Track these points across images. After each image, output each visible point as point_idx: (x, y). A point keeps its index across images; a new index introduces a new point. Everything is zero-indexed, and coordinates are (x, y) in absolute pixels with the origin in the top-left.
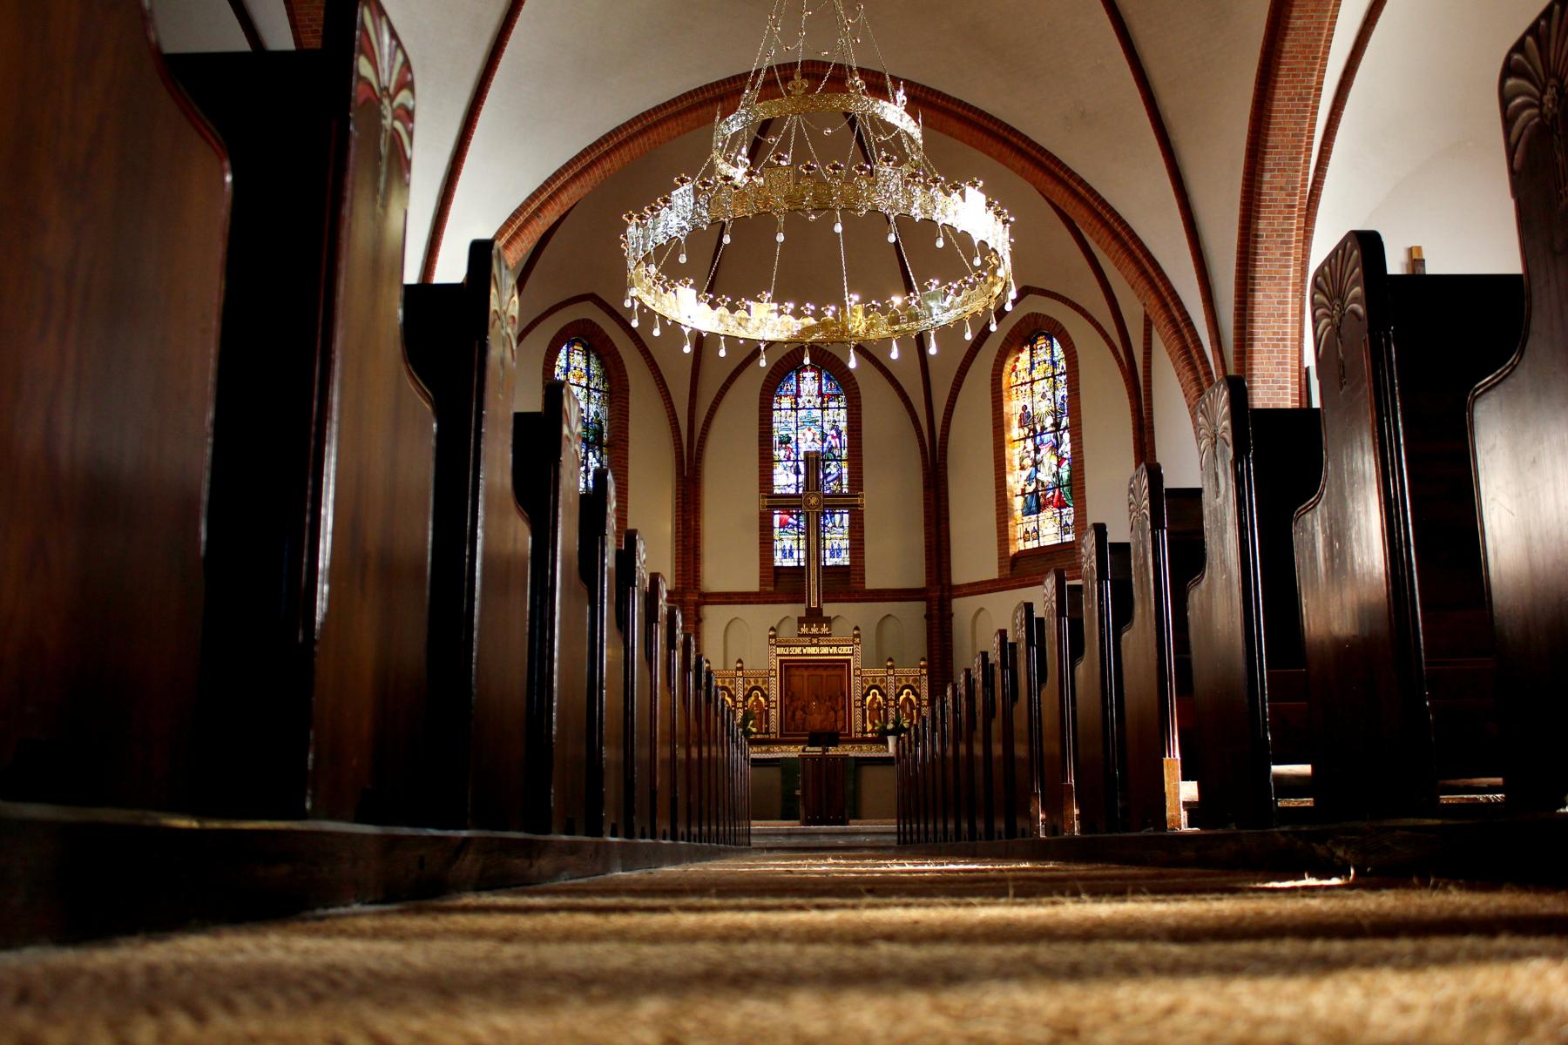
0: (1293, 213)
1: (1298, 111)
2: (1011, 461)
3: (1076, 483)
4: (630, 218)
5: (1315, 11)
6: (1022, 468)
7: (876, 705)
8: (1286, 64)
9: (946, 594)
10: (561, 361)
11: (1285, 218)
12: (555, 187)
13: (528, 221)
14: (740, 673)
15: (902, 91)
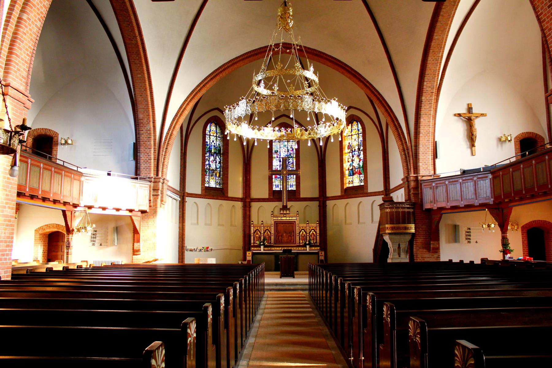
0: (433, 94)
1: (435, 64)
2: (345, 159)
3: (365, 167)
4: (227, 107)
5: (441, 34)
6: (348, 162)
7: (303, 235)
8: (432, 50)
9: (325, 199)
10: (208, 129)
12: (205, 83)
13: (196, 93)
14: (262, 225)
15: (312, 67)
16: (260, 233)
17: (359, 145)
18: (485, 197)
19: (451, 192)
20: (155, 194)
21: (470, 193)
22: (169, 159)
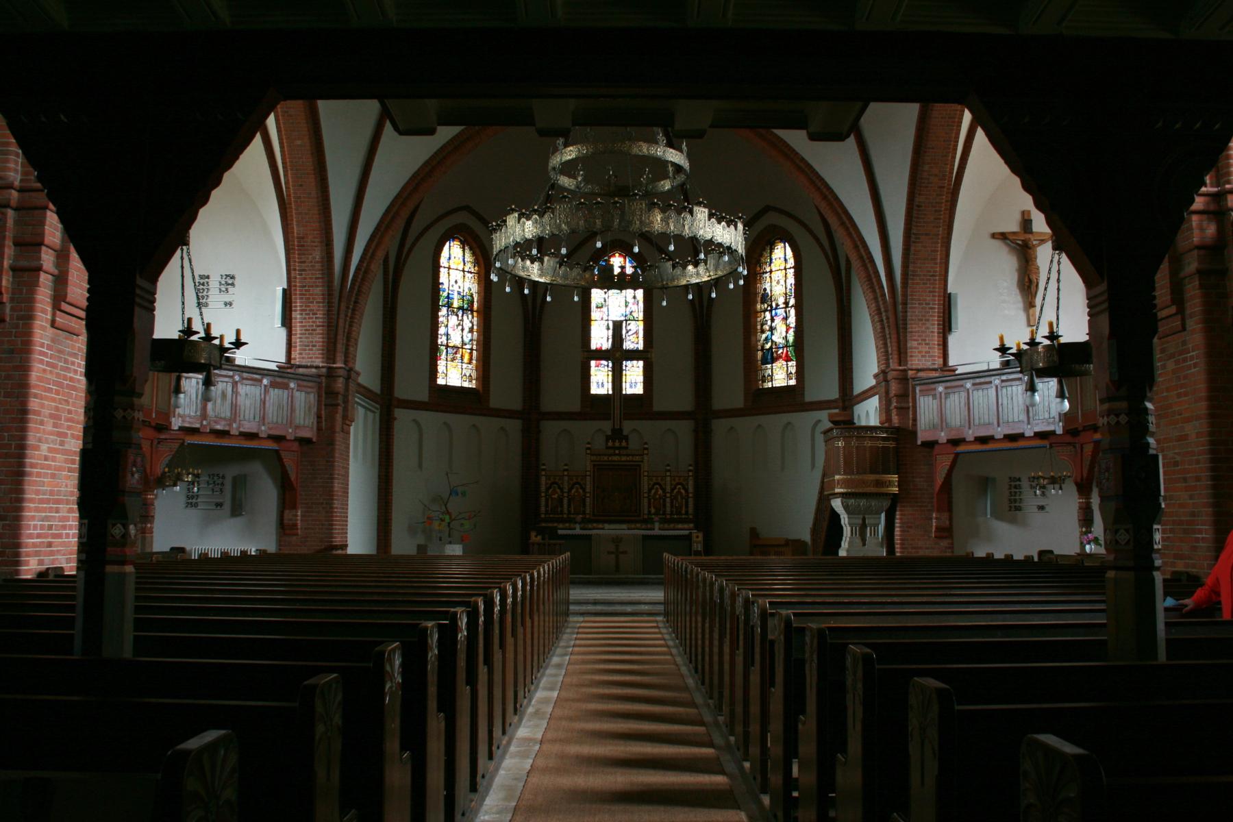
1: (948, 125)
7: (657, 496)
11: (937, 195)
16: (562, 489)
17: (786, 294)
18: (1047, 420)
19: (976, 403)
20: (23, 263)
21: (1016, 409)
22: (360, 326)
